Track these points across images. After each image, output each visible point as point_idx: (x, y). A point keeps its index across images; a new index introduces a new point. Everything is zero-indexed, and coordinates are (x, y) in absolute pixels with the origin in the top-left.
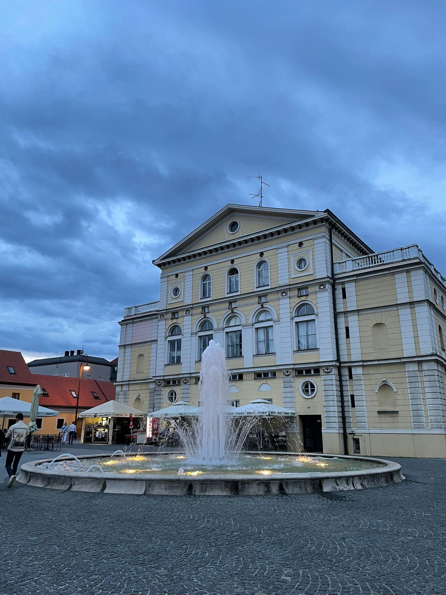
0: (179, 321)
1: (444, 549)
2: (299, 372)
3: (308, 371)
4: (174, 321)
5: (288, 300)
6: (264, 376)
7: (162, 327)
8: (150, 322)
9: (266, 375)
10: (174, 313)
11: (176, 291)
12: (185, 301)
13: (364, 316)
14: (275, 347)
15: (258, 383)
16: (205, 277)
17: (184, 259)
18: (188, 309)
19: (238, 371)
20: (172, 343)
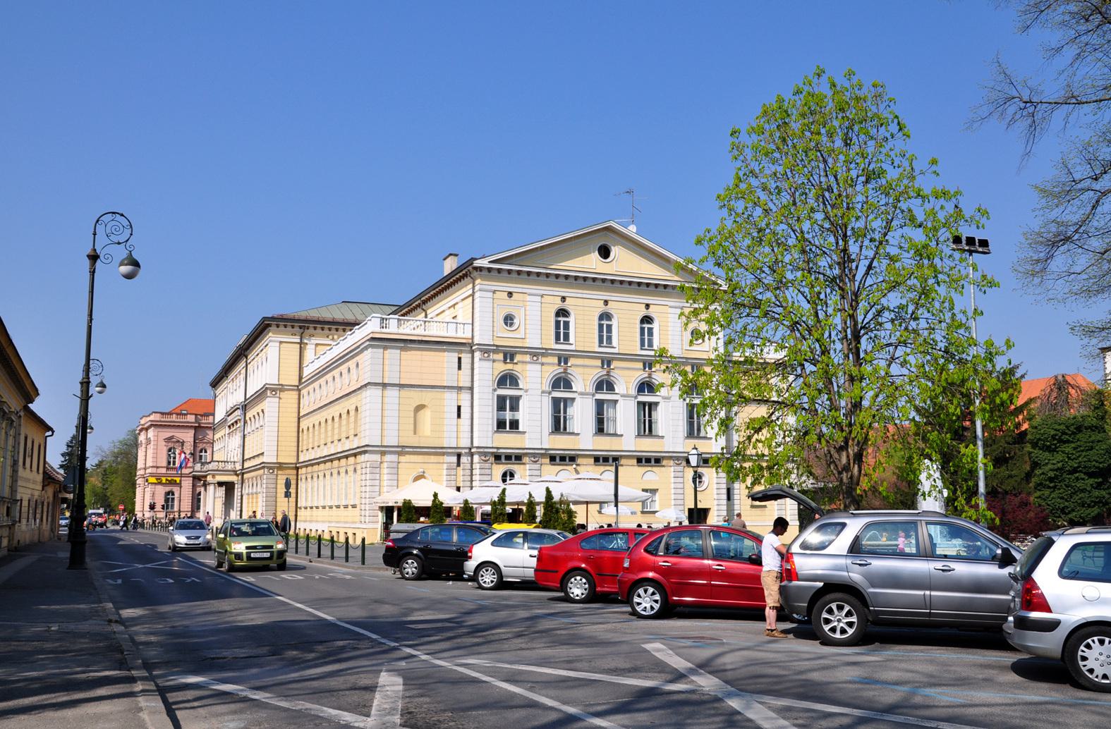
0: (518, 368)
1: (1072, 599)
2: (498, 458)
3: (508, 457)
4: (510, 366)
5: (538, 367)
6: (560, 460)
7: (486, 372)
8: (419, 353)
9: (648, 460)
10: (509, 356)
11: (509, 320)
12: (528, 340)
13: (406, 393)
14: (660, 428)
15: (642, 470)
16: (647, 319)
17: (529, 273)
18: (537, 354)
19: (517, 451)
20: (642, 405)
